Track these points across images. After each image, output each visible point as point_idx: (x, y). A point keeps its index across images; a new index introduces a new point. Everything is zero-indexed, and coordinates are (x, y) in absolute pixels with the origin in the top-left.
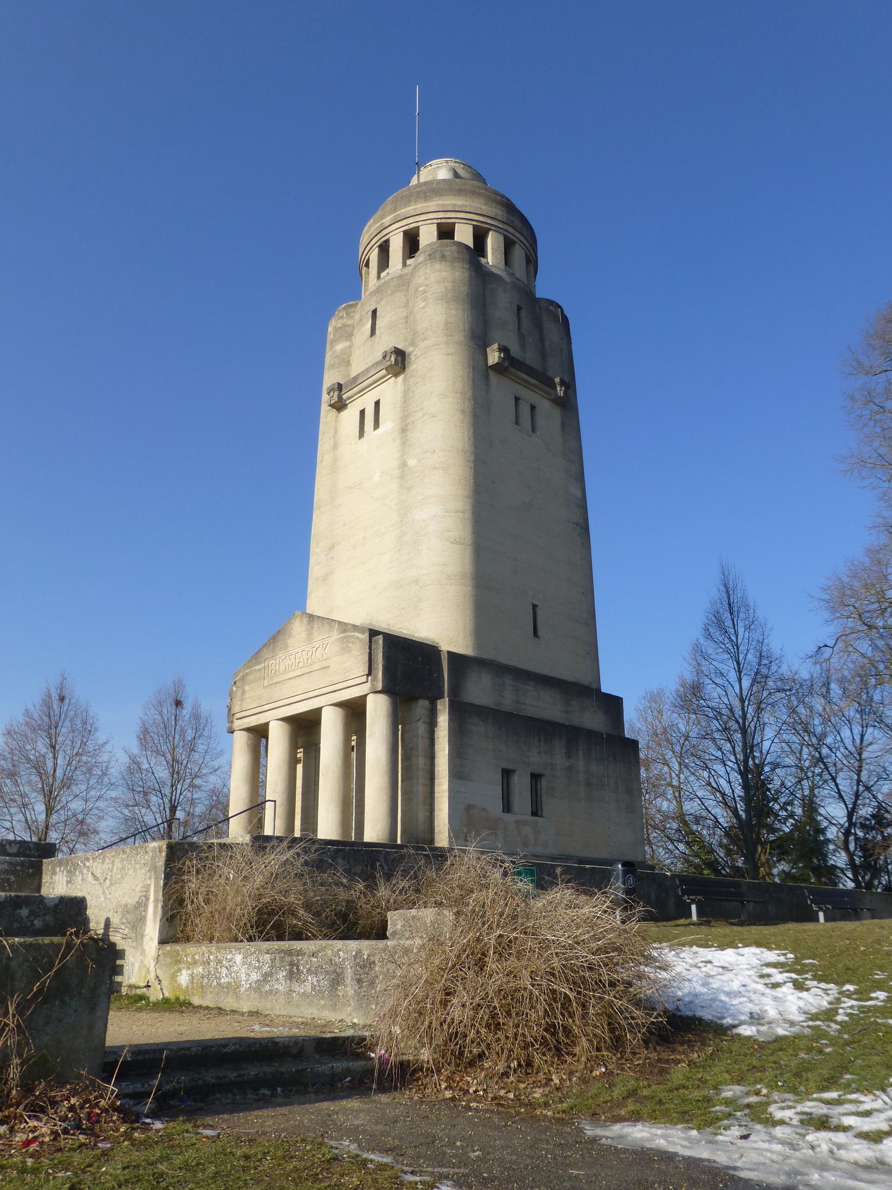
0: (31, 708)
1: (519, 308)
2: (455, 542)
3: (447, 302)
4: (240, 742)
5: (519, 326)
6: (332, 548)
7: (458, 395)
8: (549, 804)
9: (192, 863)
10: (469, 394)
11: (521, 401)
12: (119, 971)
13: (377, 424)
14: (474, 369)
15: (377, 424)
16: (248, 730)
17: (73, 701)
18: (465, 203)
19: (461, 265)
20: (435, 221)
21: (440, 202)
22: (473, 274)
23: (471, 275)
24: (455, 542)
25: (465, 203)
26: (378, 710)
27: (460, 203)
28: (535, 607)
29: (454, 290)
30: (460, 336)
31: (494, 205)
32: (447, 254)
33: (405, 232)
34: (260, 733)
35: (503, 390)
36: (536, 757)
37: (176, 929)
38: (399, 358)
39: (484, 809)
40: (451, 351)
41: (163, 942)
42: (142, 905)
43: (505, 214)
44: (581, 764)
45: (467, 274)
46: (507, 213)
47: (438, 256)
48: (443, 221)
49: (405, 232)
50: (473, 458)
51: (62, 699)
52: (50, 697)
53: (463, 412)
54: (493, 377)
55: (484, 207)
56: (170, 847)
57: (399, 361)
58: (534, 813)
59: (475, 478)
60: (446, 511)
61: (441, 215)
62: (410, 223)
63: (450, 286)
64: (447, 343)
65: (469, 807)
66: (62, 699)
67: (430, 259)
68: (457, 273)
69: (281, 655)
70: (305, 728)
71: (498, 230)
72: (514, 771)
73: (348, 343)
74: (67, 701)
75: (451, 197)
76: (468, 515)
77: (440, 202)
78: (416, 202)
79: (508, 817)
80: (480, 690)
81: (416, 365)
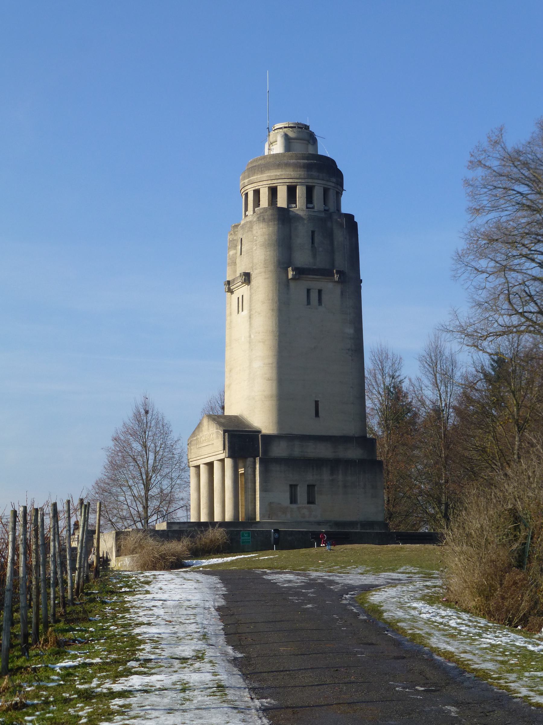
0: (127, 421)
1: (313, 232)
2: (269, 380)
3: (265, 247)
4: (192, 471)
5: (313, 243)
6: (230, 371)
7: (270, 301)
8: (318, 498)
9: (122, 536)
10: (276, 299)
11: (311, 291)
12: (109, 564)
13: (242, 311)
14: (279, 283)
15: (242, 311)
16: (195, 467)
17: (155, 412)
18: (281, 173)
19: (273, 223)
20: (267, 186)
21: (269, 174)
22: (280, 226)
23: (279, 227)
24: (269, 380)
25: (281, 173)
26: (228, 462)
27: (278, 174)
28: (317, 403)
29: (269, 240)
30: (271, 267)
31: (299, 169)
32: (266, 217)
33: (254, 191)
34: (198, 467)
35: (298, 291)
36: (311, 477)
37: (119, 553)
38: (247, 278)
39: (279, 504)
40: (267, 276)
41: (116, 557)
42: (112, 547)
43: (306, 173)
44: (340, 477)
45: (276, 228)
46: (308, 171)
47: (261, 219)
48: (271, 185)
49: (254, 191)
50: (278, 334)
51: (147, 412)
52: (140, 413)
53: (273, 310)
54: (292, 284)
55: (292, 173)
56: (116, 532)
57: (247, 278)
58: (309, 503)
59: (279, 345)
60: (264, 364)
61: (270, 182)
62: (255, 186)
63: (266, 237)
64: (265, 272)
65: (271, 503)
66: (147, 412)
67: (258, 220)
68: (271, 228)
69: (201, 435)
70: (210, 465)
71: (301, 184)
72: (296, 485)
73: (235, 251)
74: (150, 412)
75: (274, 171)
76: (275, 365)
77: (269, 174)
78: (257, 174)
79: (294, 506)
80: (279, 450)
81: (254, 282)
